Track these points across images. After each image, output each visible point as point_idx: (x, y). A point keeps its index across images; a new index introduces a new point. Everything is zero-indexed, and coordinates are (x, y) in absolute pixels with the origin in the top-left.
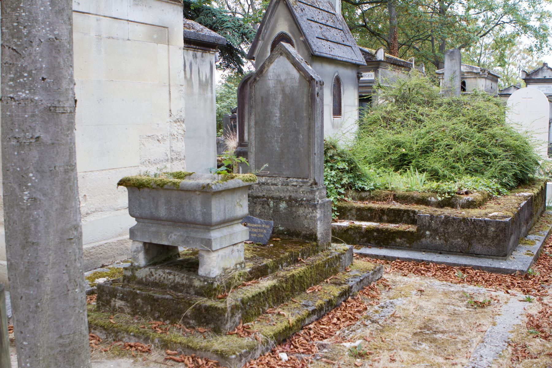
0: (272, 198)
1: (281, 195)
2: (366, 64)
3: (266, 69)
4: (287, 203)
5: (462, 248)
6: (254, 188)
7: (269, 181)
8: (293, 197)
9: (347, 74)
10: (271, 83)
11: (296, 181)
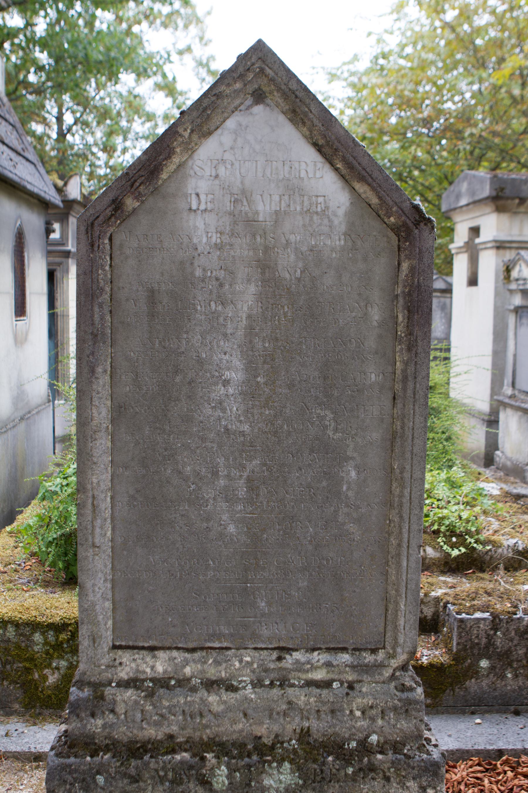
0: (222, 748)
1: (261, 730)
2: (61, 205)
3: (176, 160)
4: (298, 768)
6: (121, 709)
7: (188, 670)
8: (316, 735)
9: (33, 221)
10: (202, 229)
11: (328, 664)
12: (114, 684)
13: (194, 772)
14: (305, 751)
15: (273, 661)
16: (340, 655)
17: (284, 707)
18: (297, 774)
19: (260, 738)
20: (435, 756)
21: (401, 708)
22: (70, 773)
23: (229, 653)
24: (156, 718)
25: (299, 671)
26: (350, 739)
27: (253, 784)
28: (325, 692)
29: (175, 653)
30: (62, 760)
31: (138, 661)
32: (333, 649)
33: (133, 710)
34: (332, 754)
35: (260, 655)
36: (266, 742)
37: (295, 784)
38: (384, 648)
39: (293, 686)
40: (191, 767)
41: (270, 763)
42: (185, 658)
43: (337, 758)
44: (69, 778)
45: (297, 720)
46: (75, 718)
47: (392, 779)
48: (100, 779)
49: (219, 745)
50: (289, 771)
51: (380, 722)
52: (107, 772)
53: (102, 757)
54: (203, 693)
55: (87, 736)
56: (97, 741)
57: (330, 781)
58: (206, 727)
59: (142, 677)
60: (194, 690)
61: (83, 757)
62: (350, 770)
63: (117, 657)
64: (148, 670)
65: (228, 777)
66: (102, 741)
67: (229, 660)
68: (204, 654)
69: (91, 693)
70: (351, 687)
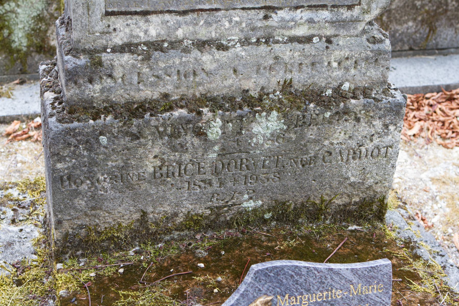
0: (215, 103)
1: (249, 85)
5: (414, 41)
6: (118, 73)
7: (180, 33)
8: (297, 86)
11: (311, 21)
12: (109, 50)
13: (191, 126)
14: (289, 100)
15: (260, 20)
16: (320, 11)
17: (271, 62)
18: (283, 121)
19: (247, 91)
20: (398, 98)
21: (372, 58)
22: (74, 136)
23: (219, 14)
24: (152, 79)
25: (284, 28)
26: (326, 88)
27: (243, 132)
28: (307, 46)
29: (167, 17)
30: (65, 125)
31: (132, 26)
32: (315, 6)
33: (130, 74)
34: (312, 102)
35: (248, 15)
36: (252, 94)
37: (280, 129)
38: (360, 4)
39: (277, 42)
40: (189, 122)
41: (260, 112)
42: (177, 21)
43: (317, 104)
44: (73, 141)
45: (282, 73)
46: (73, 85)
47: (362, 119)
48: (103, 140)
49: (211, 100)
50: (276, 119)
51: (353, 71)
52: (110, 132)
53: (105, 119)
54: (195, 53)
55: (86, 101)
56: (95, 105)
57: (310, 125)
58: (199, 84)
59: (136, 42)
60: (186, 50)
61: (86, 120)
62: (328, 115)
63: (110, 23)
64: (142, 34)
65: (221, 128)
66: (100, 105)
67: (219, 21)
68: (195, 15)
69: (88, 60)
70: (329, 41)
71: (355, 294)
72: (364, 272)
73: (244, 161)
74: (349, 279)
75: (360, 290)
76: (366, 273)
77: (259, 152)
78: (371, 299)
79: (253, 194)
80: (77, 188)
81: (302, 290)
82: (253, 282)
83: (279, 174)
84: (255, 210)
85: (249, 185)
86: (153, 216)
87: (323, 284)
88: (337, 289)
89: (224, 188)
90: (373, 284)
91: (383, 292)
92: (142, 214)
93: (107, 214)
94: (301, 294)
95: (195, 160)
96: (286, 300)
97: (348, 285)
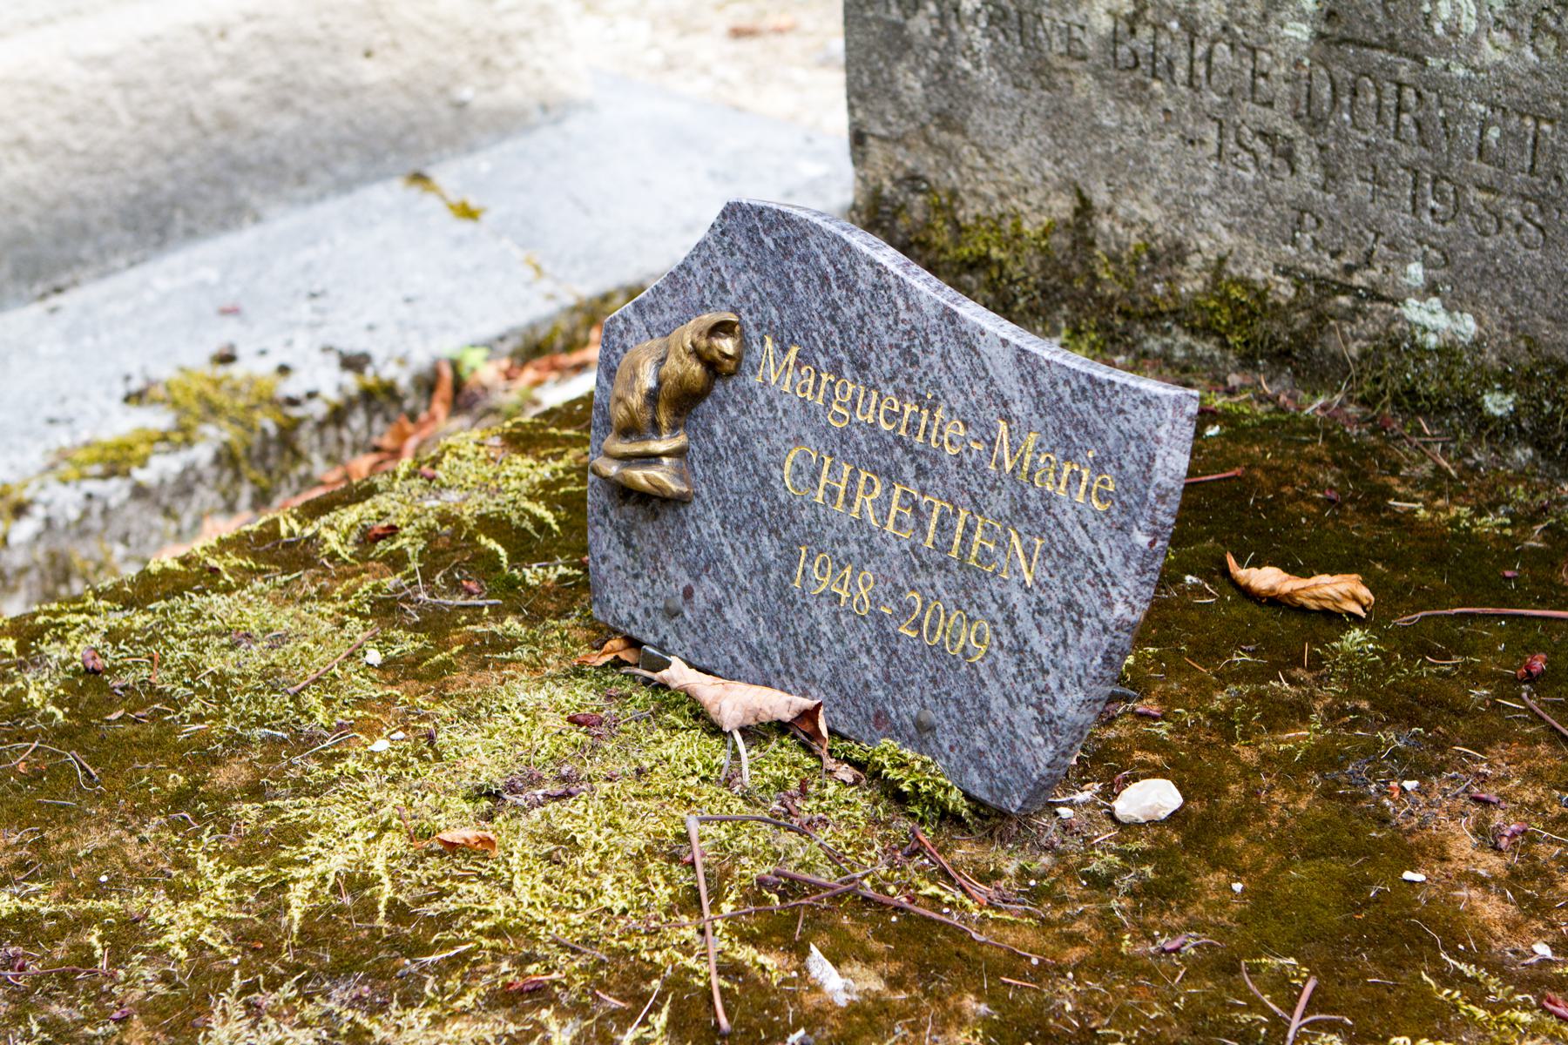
71: (1008, 466)
72: (1061, 389)
73: (1409, 96)
74: (1002, 387)
75: (1028, 457)
76: (1065, 391)
77: (1461, 72)
78: (1059, 525)
79: (1443, 272)
80: (901, 20)
81: (841, 355)
82: (712, 243)
83: (1541, 210)
84: (1448, 353)
85: (1427, 218)
86: (1112, 228)
87: (912, 365)
88: (951, 410)
89: (1339, 198)
90: (1082, 459)
91: (1107, 513)
92: (1078, 204)
93: (980, 162)
94: (836, 369)
95: (1239, 31)
96: (787, 367)
97: (991, 413)
